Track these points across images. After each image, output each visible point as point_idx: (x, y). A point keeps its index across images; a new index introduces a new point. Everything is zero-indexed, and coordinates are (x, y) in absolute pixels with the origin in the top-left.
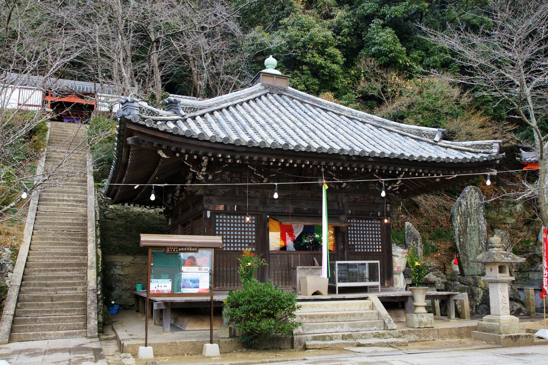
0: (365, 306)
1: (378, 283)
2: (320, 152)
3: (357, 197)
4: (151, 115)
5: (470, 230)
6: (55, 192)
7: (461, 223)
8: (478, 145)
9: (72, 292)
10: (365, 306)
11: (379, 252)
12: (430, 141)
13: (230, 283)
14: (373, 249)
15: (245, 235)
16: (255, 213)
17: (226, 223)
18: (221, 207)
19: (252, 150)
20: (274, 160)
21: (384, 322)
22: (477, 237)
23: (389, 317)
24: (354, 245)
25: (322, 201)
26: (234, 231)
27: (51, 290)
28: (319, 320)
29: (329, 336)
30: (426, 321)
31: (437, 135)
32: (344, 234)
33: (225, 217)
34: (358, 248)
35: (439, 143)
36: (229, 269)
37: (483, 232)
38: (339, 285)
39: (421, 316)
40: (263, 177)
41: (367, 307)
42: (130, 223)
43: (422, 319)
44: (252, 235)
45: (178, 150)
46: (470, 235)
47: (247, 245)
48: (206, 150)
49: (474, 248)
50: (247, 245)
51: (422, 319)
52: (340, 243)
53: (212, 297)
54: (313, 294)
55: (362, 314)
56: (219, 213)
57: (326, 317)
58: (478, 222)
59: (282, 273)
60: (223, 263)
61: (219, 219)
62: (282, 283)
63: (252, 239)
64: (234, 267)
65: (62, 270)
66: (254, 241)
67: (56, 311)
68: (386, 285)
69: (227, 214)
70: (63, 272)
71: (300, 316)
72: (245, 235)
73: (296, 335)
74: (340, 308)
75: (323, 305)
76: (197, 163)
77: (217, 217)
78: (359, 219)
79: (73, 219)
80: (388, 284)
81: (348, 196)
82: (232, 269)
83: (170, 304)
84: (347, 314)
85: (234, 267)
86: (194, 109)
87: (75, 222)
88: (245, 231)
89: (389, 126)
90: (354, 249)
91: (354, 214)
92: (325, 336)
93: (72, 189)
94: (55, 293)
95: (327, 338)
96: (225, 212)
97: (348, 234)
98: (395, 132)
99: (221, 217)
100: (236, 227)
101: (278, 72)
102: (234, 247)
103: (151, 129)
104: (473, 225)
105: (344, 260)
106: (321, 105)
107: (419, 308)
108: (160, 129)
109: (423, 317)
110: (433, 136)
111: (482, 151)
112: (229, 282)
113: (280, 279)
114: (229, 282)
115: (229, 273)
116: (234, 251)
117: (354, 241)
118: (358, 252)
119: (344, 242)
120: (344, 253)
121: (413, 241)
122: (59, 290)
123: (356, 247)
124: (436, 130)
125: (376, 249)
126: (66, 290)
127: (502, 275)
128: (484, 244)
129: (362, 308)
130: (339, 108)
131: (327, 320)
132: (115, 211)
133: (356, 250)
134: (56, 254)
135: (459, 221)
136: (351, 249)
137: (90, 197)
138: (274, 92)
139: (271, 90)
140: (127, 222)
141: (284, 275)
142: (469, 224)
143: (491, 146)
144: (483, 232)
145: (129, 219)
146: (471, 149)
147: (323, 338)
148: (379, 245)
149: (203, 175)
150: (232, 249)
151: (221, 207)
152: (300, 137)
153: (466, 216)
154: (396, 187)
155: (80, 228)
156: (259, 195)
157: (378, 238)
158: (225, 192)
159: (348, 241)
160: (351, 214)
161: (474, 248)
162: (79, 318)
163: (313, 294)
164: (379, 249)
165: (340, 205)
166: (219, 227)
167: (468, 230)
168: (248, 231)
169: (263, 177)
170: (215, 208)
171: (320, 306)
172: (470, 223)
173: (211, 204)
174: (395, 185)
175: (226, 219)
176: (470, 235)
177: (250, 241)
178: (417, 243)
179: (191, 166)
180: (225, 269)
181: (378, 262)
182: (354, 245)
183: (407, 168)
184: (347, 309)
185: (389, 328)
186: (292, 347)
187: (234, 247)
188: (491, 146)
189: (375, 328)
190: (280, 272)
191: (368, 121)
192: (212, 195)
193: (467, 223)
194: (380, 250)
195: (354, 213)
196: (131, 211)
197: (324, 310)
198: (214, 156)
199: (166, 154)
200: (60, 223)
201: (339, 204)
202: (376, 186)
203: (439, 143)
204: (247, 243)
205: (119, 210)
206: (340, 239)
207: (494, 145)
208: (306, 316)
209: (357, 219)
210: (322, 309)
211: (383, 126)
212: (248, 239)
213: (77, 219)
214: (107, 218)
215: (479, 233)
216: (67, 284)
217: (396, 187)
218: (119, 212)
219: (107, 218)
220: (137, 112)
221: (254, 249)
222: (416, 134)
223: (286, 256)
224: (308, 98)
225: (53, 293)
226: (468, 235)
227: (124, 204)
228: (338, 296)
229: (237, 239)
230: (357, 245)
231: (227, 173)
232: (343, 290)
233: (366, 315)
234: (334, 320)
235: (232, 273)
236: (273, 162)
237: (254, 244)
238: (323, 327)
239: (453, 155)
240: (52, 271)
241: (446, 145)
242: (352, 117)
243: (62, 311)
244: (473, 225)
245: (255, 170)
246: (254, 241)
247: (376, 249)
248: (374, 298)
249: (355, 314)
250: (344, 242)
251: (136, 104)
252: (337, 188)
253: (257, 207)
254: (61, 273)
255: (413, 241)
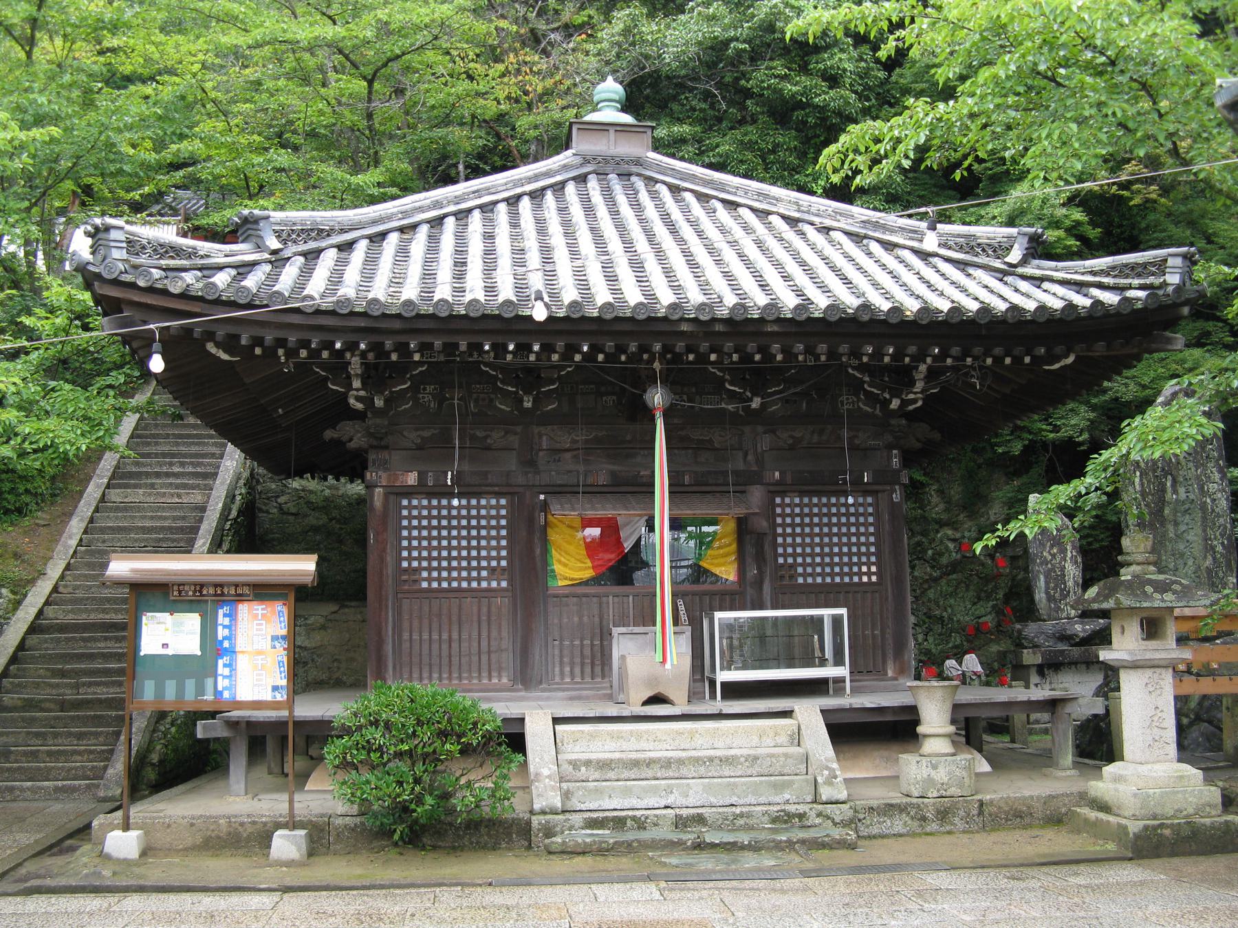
0: (776, 734)
1: (843, 671)
2: (608, 316)
3: (798, 434)
4: (172, 258)
5: (1175, 511)
6: (157, 455)
7: (1143, 494)
8: (1126, 265)
9: (112, 690)
10: (776, 734)
11: (870, 583)
12: (998, 264)
13: (470, 671)
14: (851, 574)
15: (479, 548)
16: (505, 490)
17: (430, 517)
18: (412, 479)
19: (452, 326)
20: (585, 349)
21: (816, 780)
22: (1200, 531)
23: (835, 766)
24: (794, 566)
25: (654, 448)
26: (449, 538)
27: (67, 685)
28: (626, 774)
29: (634, 818)
30: (946, 780)
31: (1016, 246)
32: (760, 537)
33: (797, 500)
34: (805, 575)
35: (1020, 270)
36: (435, 637)
37: (1218, 516)
38: (723, 676)
39: (936, 763)
40: (888, 396)
41: (783, 739)
42: (338, 521)
43: (933, 773)
44: (498, 548)
45: (305, 344)
46: (1176, 524)
47: (484, 573)
48: (352, 337)
49: (1190, 562)
50: (484, 573)
51: (933, 773)
52: (749, 560)
53: (291, 711)
54: (646, 703)
55: (756, 758)
56: (409, 492)
57: (648, 765)
58: (1201, 488)
59: (582, 645)
60: (421, 623)
61: (783, 505)
62: (582, 672)
63: (499, 559)
64: (450, 631)
65: (106, 639)
66: (504, 563)
67: (56, 735)
68: (890, 673)
69: (430, 495)
70: (109, 644)
71: (570, 762)
72: (479, 548)
73: (543, 812)
74: (699, 741)
75: (647, 732)
76: (339, 367)
77: (778, 500)
78: (811, 494)
79: (175, 519)
80: (894, 672)
81: (773, 432)
82: (445, 636)
83: (244, 725)
84: (711, 759)
85: (450, 631)
86: (322, 233)
87: (180, 524)
88: (479, 538)
89: (892, 231)
90: (793, 577)
91: (789, 481)
92: (625, 818)
93: (197, 448)
94: (75, 691)
95: (629, 822)
96: (421, 490)
97: (775, 535)
98: (905, 247)
99: (483, 502)
100: (798, 525)
101: (627, 119)
102: (449, 579)
103: (151, 290)
104: (1183, 496)
105: (761, 608)
106: (724, 191)
107: (932, 740)
108: (172, 290)
109: (935, 767)
110: (1000, 250)
111: (1136, 282)
112: (436, 669)
113: (578, 660)
114: (436, 669)
115: (435, 646)
116: (450, 590)
117: (794, 555)
118: (806, 585)
119: (760, 559)
120: (761, 589)
121: (1052, 546)
122: (84, 684)
123: (800, 570)
124: (1013, 231)
125: (860, 574)
126: (98, 684)
127: (1152, 644)
128: (1219, 548)
129: (769, 741)
130: (766, 196)
131: (650, 773)
132: (302, 494)
133: (801, 580)
134: (108, 600)
135: (1138, 488)
136: (782, 577)
137: (228, 463)
138: (608, 169)
139: (603, 167)
140: (331, 520)
141: (587, 652)
142: (1170, 497)
143: (1161, 265)
144: (1218, 516)
145: (335, 513)
146: (1106, 280)
147: (619, 823)
148: (869, 564)
149: (358, 399)
150: (435, 585)
151: (412, 479)
152: (953, 283)
153: (1158, 473)
154: (915, 401)
155: (182, 539)
156: (514, 441)
157: (867, 544)
158: (423, 438)
159: (776, 555)
160: (779, 483)
161: (1190, 562)
162: (103, 751)
163: (646, 703)
164: (869, 574)
165: (750, 457)
166: (410, 528)
167: (1167, 511)
168: (488, 538)
169: (749, 394)
170: (396, 479)
171: (639, 736)
172: (1175, 491)
173: (386, 470)
174: (911, 396)
175: (430, 508)
176: (1176, 524)
177: (494, 563)
178: (1063, 551)
179: (727, 377)
180: (426, 636)
181: (843, 611)
182: (794, 566)
183: (936, 345)
184: (720, 744)
185: (824, 798)
186: (529, 847)
187: (449, 579)
188: (1161, 265)
189: (787, 796)
190: (577, 642)
191: (835, 224)
192: (386, 447)
193: (1164, 491)
194: (874, 578)
195: (789, 480)
196: (340, 493)
197: (651, 746)
198: (377, 347)
199: (225, 351)
200: (142, 528)
201: (746, 455)
202: (859, 400)
203: (1020, 270)
204: (484, 568)
205: (311, 492)
206: (750, 550)
207: (1170, 262)
208: (588, 763)
209: (802, 494)
210: (644, 745)
211: (877, 235)
212: (489, 558)
213: (184, 518)
214: (284, 513)
215: (1204, 519)
216: (107, 672)
217: (915, 401)
218: (313, 498)
219: (284, 513)
220: (121, 254)
221: (504, 584)
222: (961, 249)
223: (595, 600)
224: (693, 178)
225: (69, 692)
226: (1171, 528)
227: (325, 479)
228: (720, 705)
229: (459, 558)
230: (804, 565)
231: (430, 388)
232: (734, 691)
233: (768, 761)
234: (671, 774)
235: (445, 646)
236: (868, 354)
237: (504, 569)
238: (627, 792)
239: (1054, 298)
240: (84, 640)
241: (1038, 273)
242: (796, 215)
243: (70, 734)
244: (1183, 496)
245: (867, 379)
246: (504, 563)
247: (860, 574)
248: (809, 714)
249: (734, 758)
250: (760, 559)
251: (114, 234)
252: (877, 411)
253: (508, 474)
254: (102, 645)
255: (1052, 546)
